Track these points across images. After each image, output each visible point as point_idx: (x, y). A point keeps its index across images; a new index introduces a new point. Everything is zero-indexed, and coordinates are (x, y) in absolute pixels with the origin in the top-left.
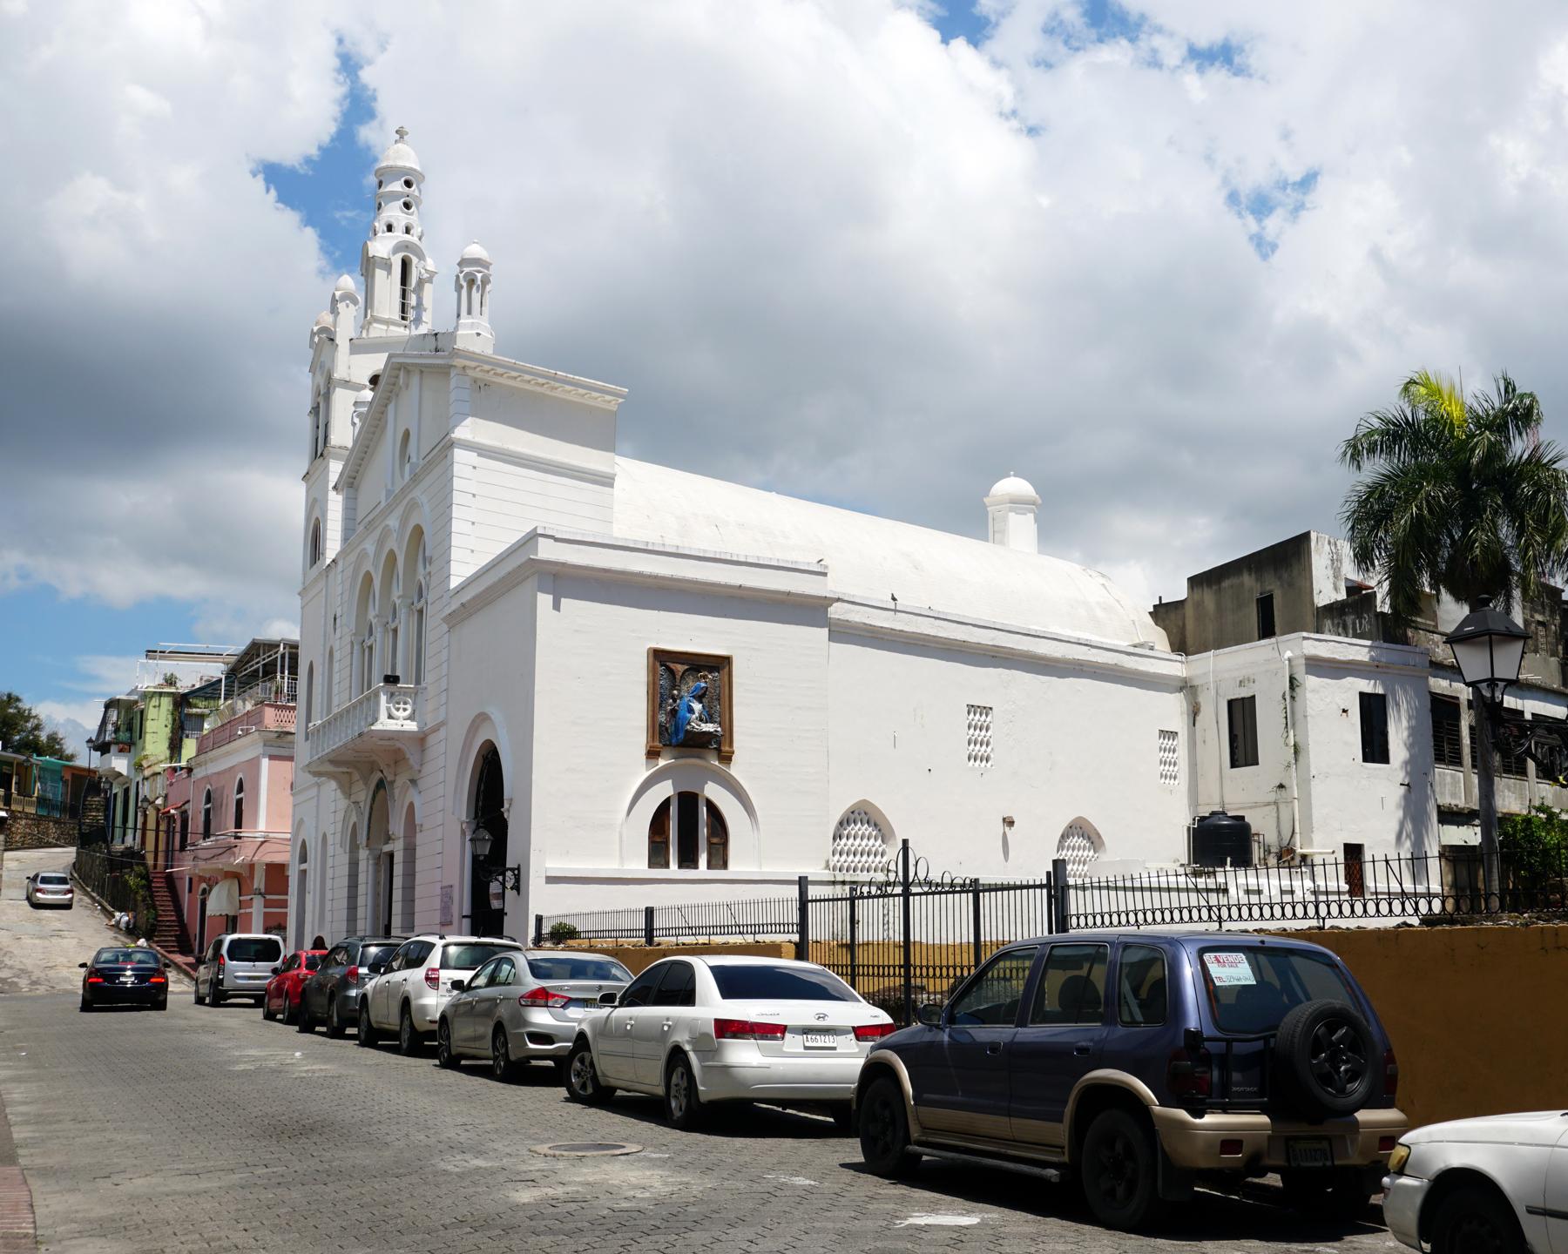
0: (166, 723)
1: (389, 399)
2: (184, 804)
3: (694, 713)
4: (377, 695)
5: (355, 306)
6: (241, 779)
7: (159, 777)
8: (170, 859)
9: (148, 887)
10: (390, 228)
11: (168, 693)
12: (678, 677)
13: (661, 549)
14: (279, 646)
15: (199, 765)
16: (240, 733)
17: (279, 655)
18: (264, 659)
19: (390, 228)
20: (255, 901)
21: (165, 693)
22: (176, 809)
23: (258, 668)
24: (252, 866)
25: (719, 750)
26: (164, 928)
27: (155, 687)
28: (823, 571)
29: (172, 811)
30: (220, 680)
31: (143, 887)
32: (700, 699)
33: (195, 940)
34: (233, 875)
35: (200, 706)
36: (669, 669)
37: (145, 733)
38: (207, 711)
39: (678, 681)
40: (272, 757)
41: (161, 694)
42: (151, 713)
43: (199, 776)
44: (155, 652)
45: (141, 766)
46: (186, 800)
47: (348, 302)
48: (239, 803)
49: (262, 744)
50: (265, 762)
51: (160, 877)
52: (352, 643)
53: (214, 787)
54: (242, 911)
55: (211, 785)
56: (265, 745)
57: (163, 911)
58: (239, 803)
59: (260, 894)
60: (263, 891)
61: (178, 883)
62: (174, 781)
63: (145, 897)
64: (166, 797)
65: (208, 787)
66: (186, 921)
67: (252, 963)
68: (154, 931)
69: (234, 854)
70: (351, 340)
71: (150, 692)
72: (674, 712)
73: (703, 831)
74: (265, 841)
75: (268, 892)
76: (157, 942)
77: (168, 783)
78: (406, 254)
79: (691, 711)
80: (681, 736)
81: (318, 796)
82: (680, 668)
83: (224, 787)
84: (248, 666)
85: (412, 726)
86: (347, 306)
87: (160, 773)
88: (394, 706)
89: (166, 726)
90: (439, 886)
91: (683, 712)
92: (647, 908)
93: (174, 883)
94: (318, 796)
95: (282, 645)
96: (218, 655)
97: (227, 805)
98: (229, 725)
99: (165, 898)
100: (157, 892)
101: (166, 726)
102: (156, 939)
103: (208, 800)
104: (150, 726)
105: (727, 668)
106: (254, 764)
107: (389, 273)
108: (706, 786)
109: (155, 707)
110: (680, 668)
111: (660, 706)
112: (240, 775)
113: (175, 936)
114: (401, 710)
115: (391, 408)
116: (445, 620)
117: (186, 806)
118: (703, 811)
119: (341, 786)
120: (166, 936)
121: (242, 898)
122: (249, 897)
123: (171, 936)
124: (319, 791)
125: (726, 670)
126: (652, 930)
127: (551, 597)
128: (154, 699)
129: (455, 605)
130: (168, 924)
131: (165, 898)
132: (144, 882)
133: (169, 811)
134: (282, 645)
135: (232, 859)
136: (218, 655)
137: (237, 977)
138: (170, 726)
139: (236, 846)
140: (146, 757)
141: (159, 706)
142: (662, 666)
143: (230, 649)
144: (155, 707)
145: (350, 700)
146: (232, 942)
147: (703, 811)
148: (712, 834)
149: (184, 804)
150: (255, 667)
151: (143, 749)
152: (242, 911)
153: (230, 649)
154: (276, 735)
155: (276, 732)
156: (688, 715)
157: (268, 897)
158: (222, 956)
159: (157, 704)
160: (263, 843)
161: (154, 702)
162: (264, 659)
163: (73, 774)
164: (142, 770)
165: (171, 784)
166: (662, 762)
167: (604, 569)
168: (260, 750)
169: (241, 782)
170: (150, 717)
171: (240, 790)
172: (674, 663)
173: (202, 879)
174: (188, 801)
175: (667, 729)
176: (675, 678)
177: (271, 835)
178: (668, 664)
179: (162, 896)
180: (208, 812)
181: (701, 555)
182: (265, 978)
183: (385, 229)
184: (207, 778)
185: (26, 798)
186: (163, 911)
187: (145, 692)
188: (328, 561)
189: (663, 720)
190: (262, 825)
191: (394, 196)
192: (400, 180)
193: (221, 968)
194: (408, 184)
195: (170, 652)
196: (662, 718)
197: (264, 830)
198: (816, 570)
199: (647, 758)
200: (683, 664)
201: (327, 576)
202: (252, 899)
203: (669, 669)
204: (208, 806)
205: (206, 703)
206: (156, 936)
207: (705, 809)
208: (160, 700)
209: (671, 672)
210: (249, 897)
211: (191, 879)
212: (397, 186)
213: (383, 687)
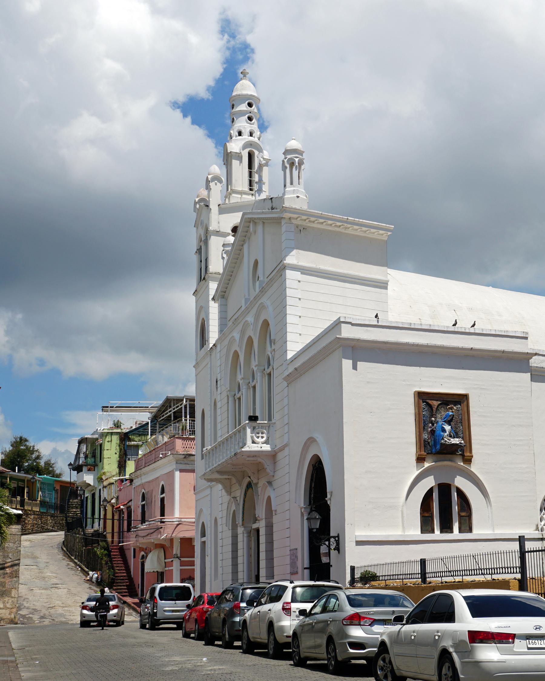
0: (116, 451)
1: (244, 241)
2: (128, 502)
3: (446, 432)
4: (244, 429)
5: (221, 184)
6: (163, 485)
7: (112, 485)
8: (121, 537)
9: (109, 555)
10: (240, 134)
11: (116, 432)
12: (434, 409)
13: (420, 327)
14: (183, 400)
15: (137, 477)
16: (161, 456)
17: (183, 406)
18: (174, 409)
19: (240, 134)
20: (174, 563)
21: (114, 432)
22: (123, 505)
23: (171, 414)
24: (171, 540)
25: (463, 455)
26: (119, 581)
27: (108, 429)
28: (525, 336)
29: (122, 507)
30: (148, 423)
31: (106, 555)
32: (449, 423)
33: (139, 588)
34: (161, 546)
35: (136, 440)
36: (428, 405)
37: (103, 458)
38: (140, 443)
39: (434, 411)
40: (181, 471)
41: (112, 434)
42: (107, 446)
43: (137, 484)
44: (108, 407)
45: (102, 479)
46: (130, 499)
47: (216, 181)
48: (162, 500)
49: (175, 462)
50: (177, 474)
51: (116, 549)
52: (228, 396)
53: (147, 491)
54: (167, 569)
55: (145, 490)
56: (177, 463)
57: (119, 570)
58: (162, 500)
59: (178, 557)
60: (179, 555)
61: (127, 552)
62: (122, 488)
63: (107, 562)
64: (117, 498)
65: (143, 491)
66: (132, 577)
67: (174, 602)
68: (114, 583)
69: (160, 532)
70: (219, 205)
71: (104, 432)
72: (433, 432)
73: (455, 508)
74: (179, 524)
75: (182, 556)
76: (115, 590)
77: (118, 489)
78: (250, 149)
79: (444, 430)
80: (438, 447)
81: (211, 494)
82: (435, 403)
83: (152, 490)
84: (164, 414)
85: (267, 448)
86: (216, 184)
87: (113, 483)
88: (256, 435)
89: (116, 453)
90: (288, 549)
91: (438, 432)
92: (421, 560)
93: (124, 552)
94: (211, 494)
95: (185, 400)
96: (145, 407)
97: (155, 501)
98: (154, 452)
99: (119, 562)
100: (114, 558)
101: (116, 453)
102: (115, 588)
103: (143, 499)
104: (106, 454)
105: (466, 401)
106: (171, 475)
107: (241, 162)
108: (456, 479)
109: (108, 442)
110: (435, 403)
111: (424, 428)
112: (162, 483)
113: (127, 586)
114: (260, 438)
115: (246, 247)
116: (285, 379)
117: (130, 504)
118: (455, 495)
119: (225, 487)
120: (121, 586)
121: (166, 561)
122: (171, 560)
123: (124, 586)
124: (211, 491)
125: (465, 403)
126: (425, 573)
127: (351, 361)
128: (108, 437)
129: (291, 369)
130: (121, 578)
131: (119, 562)
132: (106, 552)
133: (120, 507)
134: (185, 400)
135: (159, 536)
136: (145, 407)
137: (165, 611)
138: (118, 453)
139: (161, 528)
140: (104, 473)
141: (111, 441)
142: (423, 402)
143: (154, 403)
144: (108, 442)
145: (228, 432)
146: (161, 589)
147: (455, 495)
148: (461, 510)
149: (128, 502)
150: (169, 414)
151: (103, 468)
152: (167, 569)
153: (154, 403)
154: (183, 456)
155: (183, 454)
156: (442, 433)
157: (182, 559)
158: (155, 597)
159: (110, 440)
160: (178, 525)
161: (108, 438)
162: (174, 409)
163: (61, 486)
164: (103, 482)
165: (120, 490)
166: (427, 465)
167: (384, 342)
168: (174, 466)
169: (163, 487)
170: (106, 448)
171: (163, 492)
172: (431, 400)
173: (141, 549)
174: (131, 500)
175: (429, 443)
176: (432, 410)
177: (183, 520)
178: (427, 401)
179: (118, 560)
180: (143, 506)
181: (446, 329)
182: (182, 611)
183: (237, 134)
184: (142, 486)
185: (33, 502)
186: (119, 570)
187: (102, 433)
188: (211, 345)
189: (426, 437)
190: (177, 514)
191: (242, 113)
192: (245, 103)
193: (155, 606)
194: (250, 105)
195: (116, 407)
196: (425, 436)
197: (178, 517)
198: (520, 335)
199: (417, 462)
200: (437, 400)
201: (211, 355)
202: (172, 561)
203: (428, 405)
204: (144, 503)
205: (140, 438)
206: (115, 586)
207: (456, 494)
208: (111, 437)
209: (430, 406)
210: (171, 560)
211: (134, 550)
212: (243, 107)
213: (248, 423)
